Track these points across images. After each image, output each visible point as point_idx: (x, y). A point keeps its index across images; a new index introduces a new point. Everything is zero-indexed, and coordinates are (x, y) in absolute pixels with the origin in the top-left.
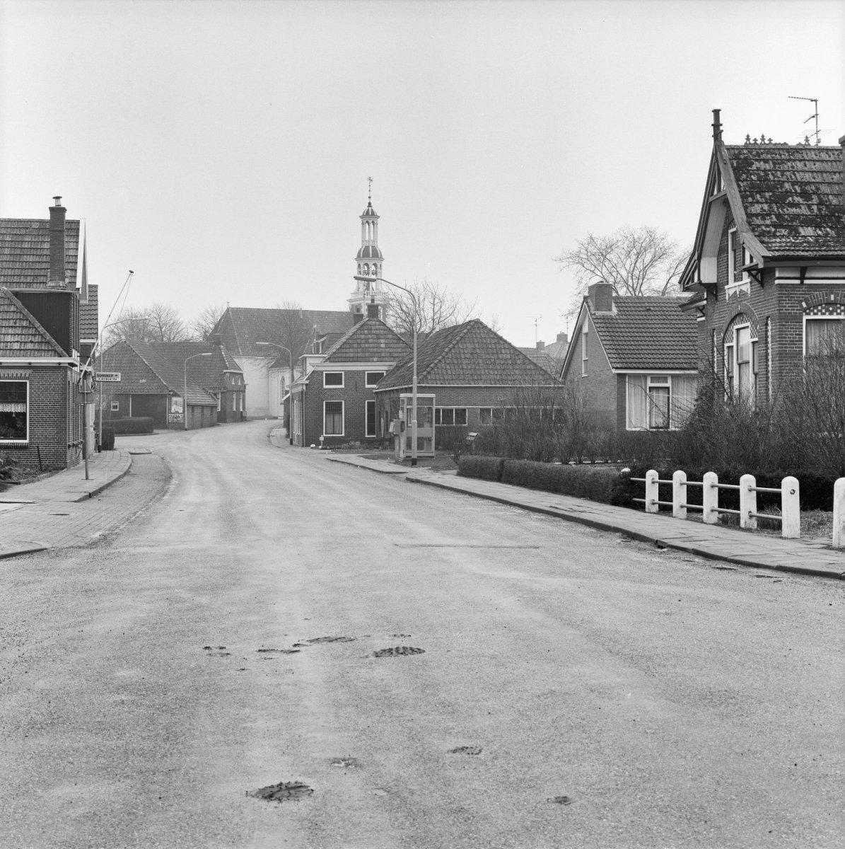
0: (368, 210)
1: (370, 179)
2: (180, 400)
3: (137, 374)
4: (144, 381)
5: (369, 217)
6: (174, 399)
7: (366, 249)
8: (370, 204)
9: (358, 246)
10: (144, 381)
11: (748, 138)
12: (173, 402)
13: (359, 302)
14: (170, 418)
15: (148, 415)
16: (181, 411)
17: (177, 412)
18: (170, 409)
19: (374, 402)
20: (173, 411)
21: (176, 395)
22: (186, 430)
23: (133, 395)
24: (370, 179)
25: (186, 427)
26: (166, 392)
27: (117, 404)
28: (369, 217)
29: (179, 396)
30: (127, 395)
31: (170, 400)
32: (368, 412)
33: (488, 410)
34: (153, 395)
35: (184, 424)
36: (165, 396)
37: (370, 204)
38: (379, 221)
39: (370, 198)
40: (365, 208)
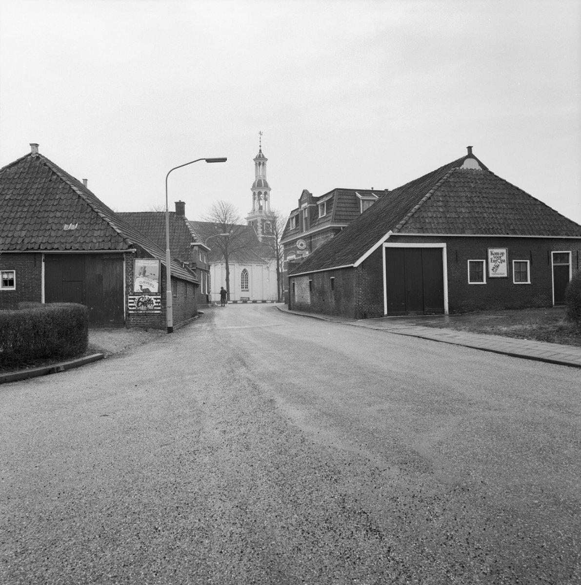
0: (260, 155)
1: (260, 133)
2: (152, 265)
3: (58, 214)
4: (72, 227)
5: (260, 160)
6: (140, 263)
7: (260, 181)
8: (260, 150)
9: (252, 180)
10: (72, 227)
11: (372, 188)
12: (137, 271)
13: (255, 219)
14: (130, 304)
15: (82, 300)
16: (154, 288)
17: (146, 292)
18: (131, 285)
19: (40, 301)
20: (137, 289)
21: (144, 255)
22: (170, 330)
23: (48, 256)
24: (260, 133)
25: (170, 324)
26: (121, 248)
27: (13, 276)
28: (260, 160)
29: (149, 257)
30: (36, 255)
31: (132, 266)
32: (552, 277)
33: (246, 288)
34: (93, 256)
35: (163, 316)
36: (118, 257)
37: (260, 150)
38: (267, 163)
39: (260, 146)
40: (257, 153)
